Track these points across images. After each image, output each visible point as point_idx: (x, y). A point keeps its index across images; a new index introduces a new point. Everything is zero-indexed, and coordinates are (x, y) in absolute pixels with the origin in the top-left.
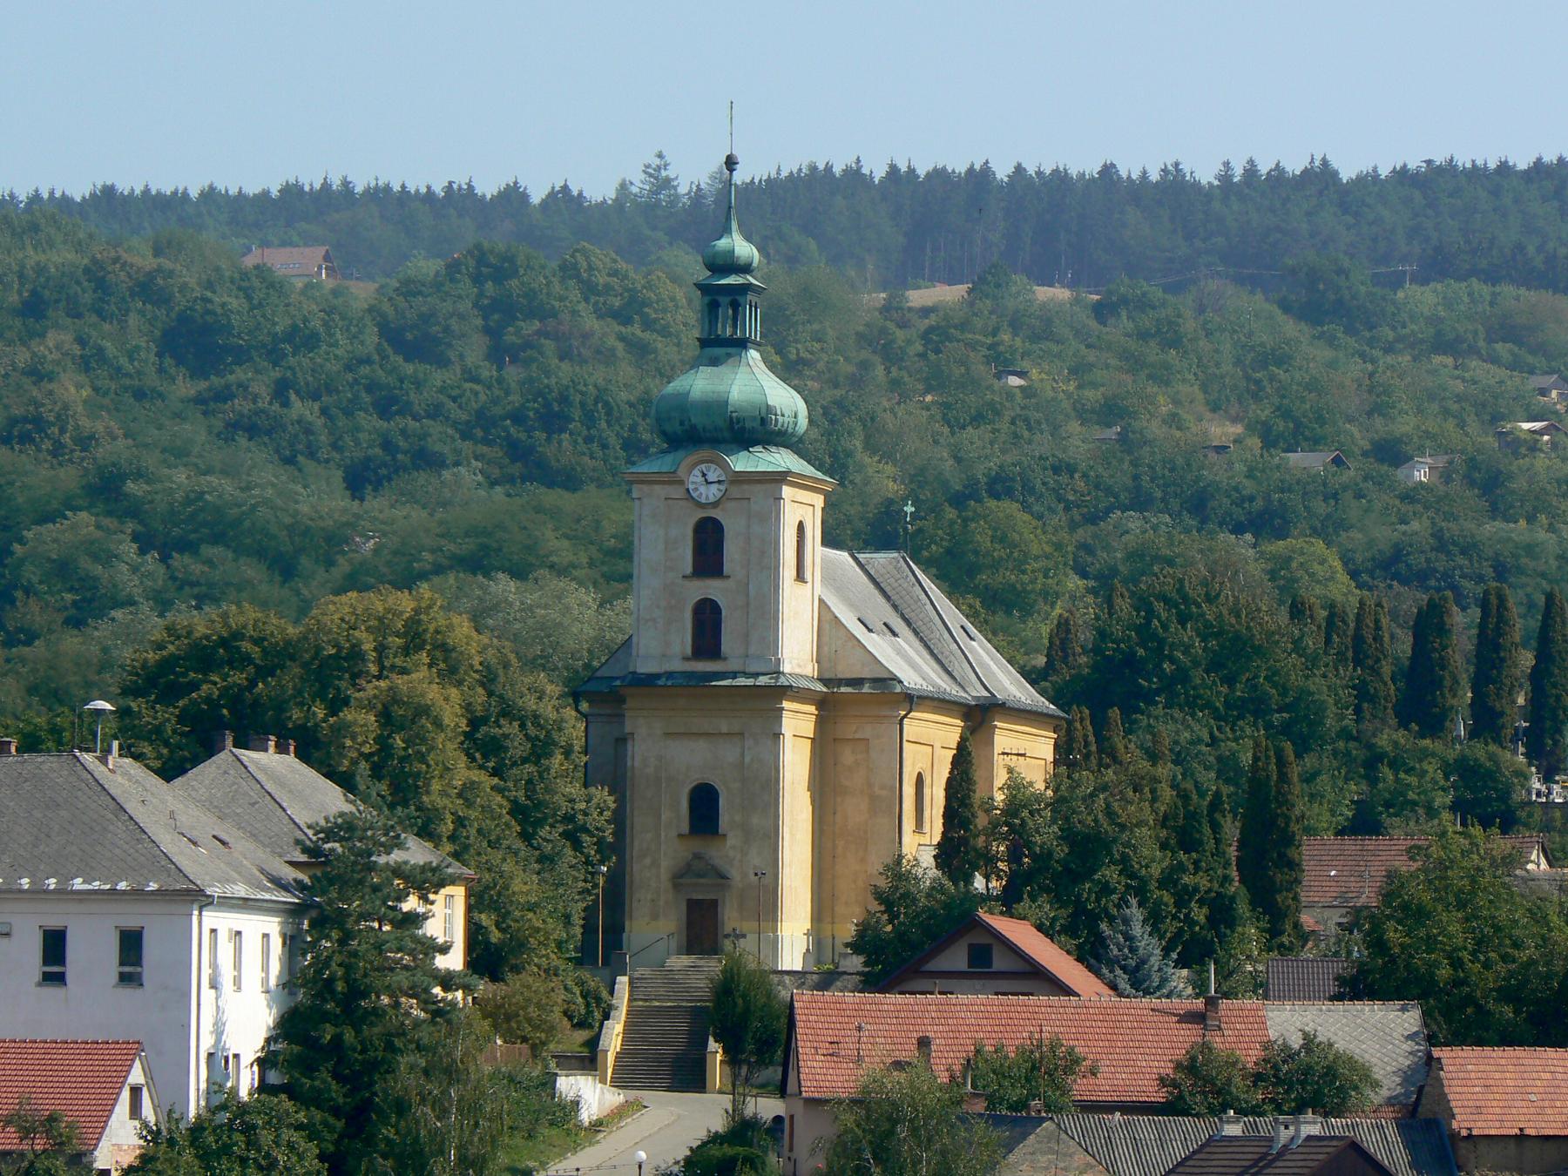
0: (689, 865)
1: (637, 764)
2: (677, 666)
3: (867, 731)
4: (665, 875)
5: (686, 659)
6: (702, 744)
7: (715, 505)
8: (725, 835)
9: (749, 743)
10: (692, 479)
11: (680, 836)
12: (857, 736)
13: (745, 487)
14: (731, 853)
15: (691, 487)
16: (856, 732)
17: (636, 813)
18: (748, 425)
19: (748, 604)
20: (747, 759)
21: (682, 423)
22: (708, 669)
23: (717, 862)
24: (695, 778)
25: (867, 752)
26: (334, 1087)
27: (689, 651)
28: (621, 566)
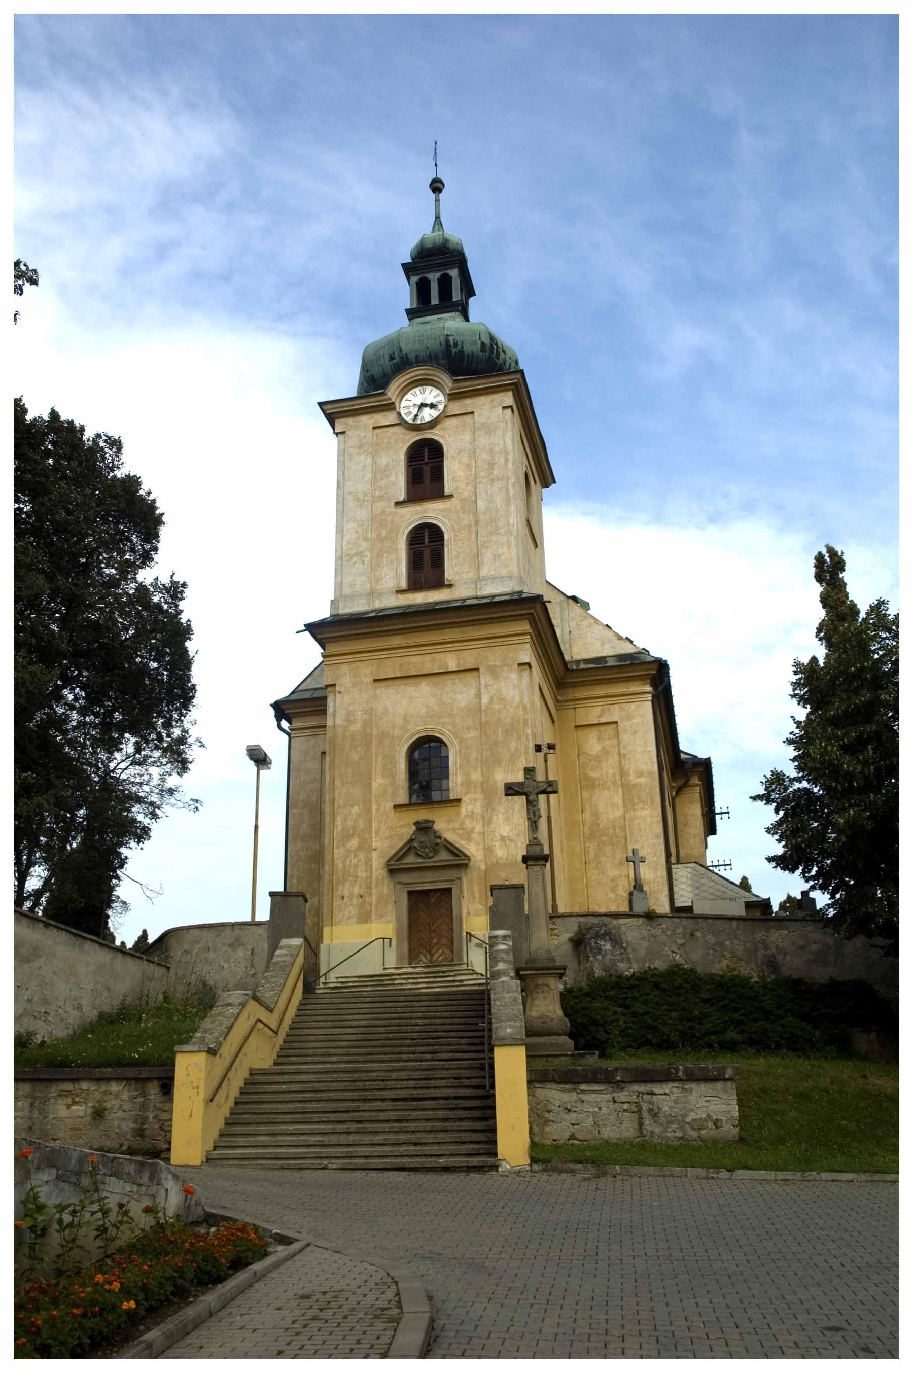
0: (411, 841)
1: (338, 722)
2: (392, 601)
3: (615, 713)
4: (378, 863)
5: (400, 592)
6: (424, 688)
7: (433, 424)
8: (459, 800)
9: (485, 678)
10: (404, 403)
11: (396, 807)
12: (602, 720)
13: (468, 401)
14: (468, 824)
15: (403, 412)
16: (600, 716)
17: (338, 783)
18: (468, 348)
19: (477, 523)
20: (485, 700)
21: (392, 358)
22: (430, 600)
23: (450, 836)
24: (417, 730)
25: (617, 735)
26: (650, 1021)
27: (404, 584)
28: (489, 1102)
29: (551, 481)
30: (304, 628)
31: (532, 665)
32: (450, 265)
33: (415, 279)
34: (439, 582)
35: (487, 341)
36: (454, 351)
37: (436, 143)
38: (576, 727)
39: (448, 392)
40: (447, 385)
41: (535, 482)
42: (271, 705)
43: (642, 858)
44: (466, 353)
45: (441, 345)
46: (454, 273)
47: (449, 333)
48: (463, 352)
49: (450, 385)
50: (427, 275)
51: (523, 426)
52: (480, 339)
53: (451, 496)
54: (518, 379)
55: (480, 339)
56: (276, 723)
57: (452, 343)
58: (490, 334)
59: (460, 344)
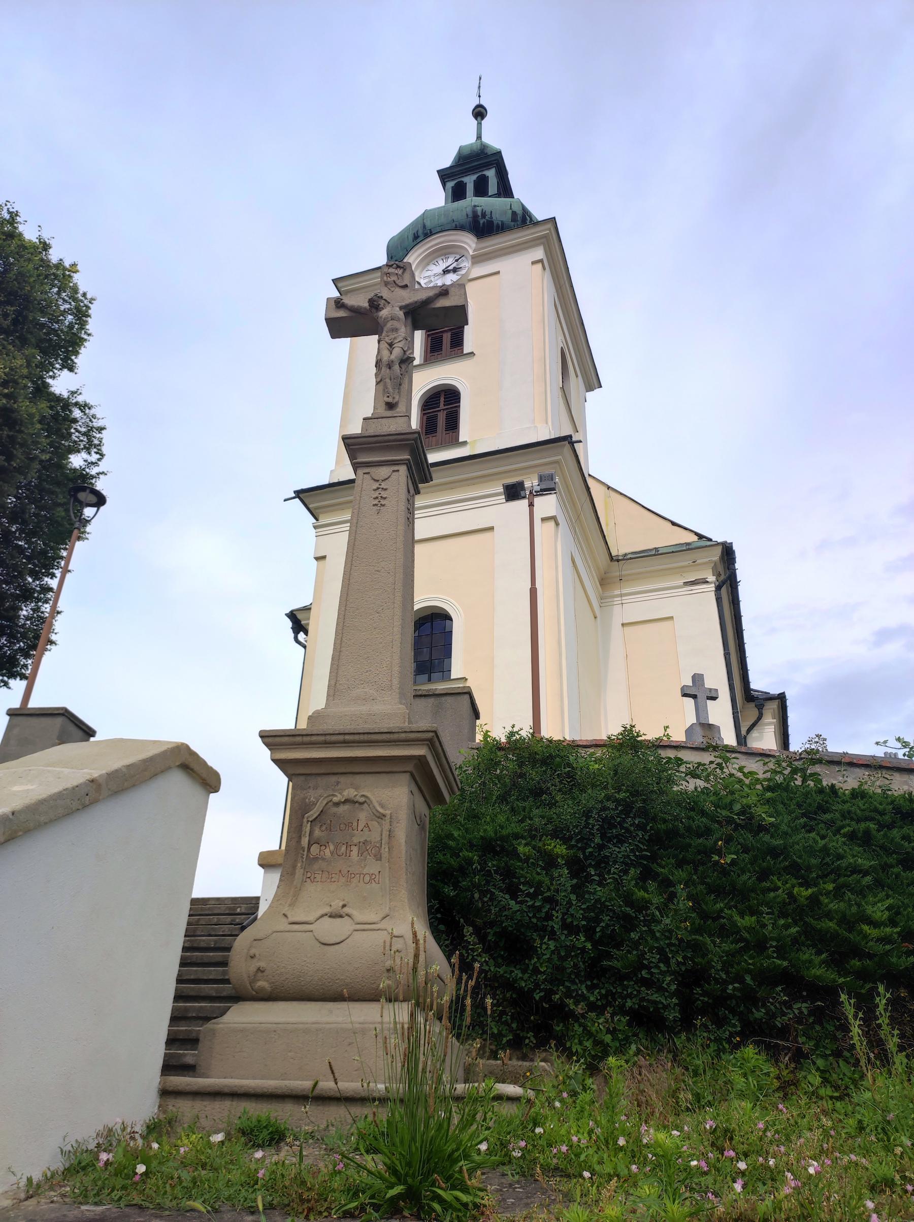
29: (596, 386)
30: (294, 495)
31: (561, 519)
32: (487, 166)
33: (451, 184)
34: (455, 442)
35: (519, 212)
36: (482, 222)
37: (480, 78)
38: (623, 625)
39: (471, 253)
40: (470, 246)
41: (577, 376)
42: (286, 615)
43: (710, 690)
44: (495, 222)
45: (467, 215)
46: (491, 173)
47: (476, 204)
48: (492, 222)
49: (474, 246)
50: (462, 179)
51: (557, 291)
52: (511, 209)
53: (472, 354)
54: (550, 229)
55: (511, 209)
56: (293, 635)
57: (479, 213)
58: (522, 205)
59: (488, 213)
